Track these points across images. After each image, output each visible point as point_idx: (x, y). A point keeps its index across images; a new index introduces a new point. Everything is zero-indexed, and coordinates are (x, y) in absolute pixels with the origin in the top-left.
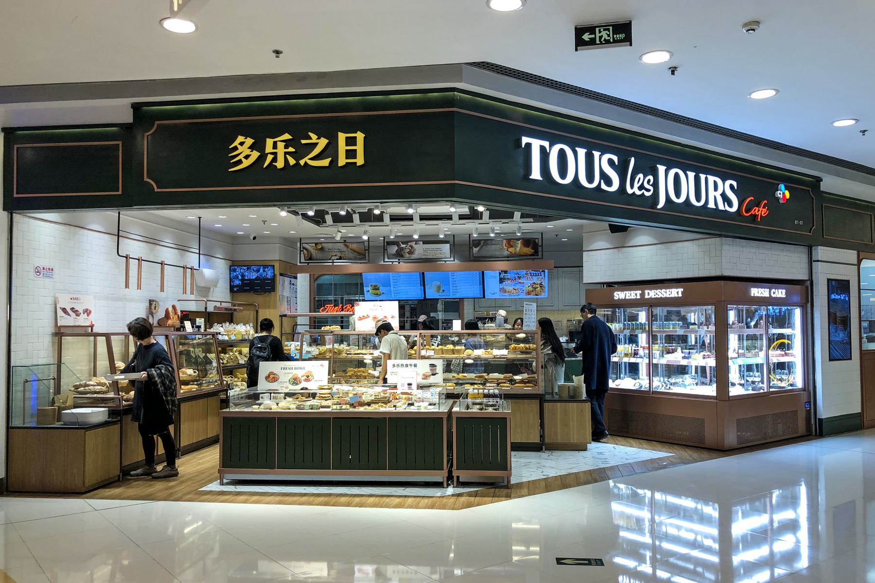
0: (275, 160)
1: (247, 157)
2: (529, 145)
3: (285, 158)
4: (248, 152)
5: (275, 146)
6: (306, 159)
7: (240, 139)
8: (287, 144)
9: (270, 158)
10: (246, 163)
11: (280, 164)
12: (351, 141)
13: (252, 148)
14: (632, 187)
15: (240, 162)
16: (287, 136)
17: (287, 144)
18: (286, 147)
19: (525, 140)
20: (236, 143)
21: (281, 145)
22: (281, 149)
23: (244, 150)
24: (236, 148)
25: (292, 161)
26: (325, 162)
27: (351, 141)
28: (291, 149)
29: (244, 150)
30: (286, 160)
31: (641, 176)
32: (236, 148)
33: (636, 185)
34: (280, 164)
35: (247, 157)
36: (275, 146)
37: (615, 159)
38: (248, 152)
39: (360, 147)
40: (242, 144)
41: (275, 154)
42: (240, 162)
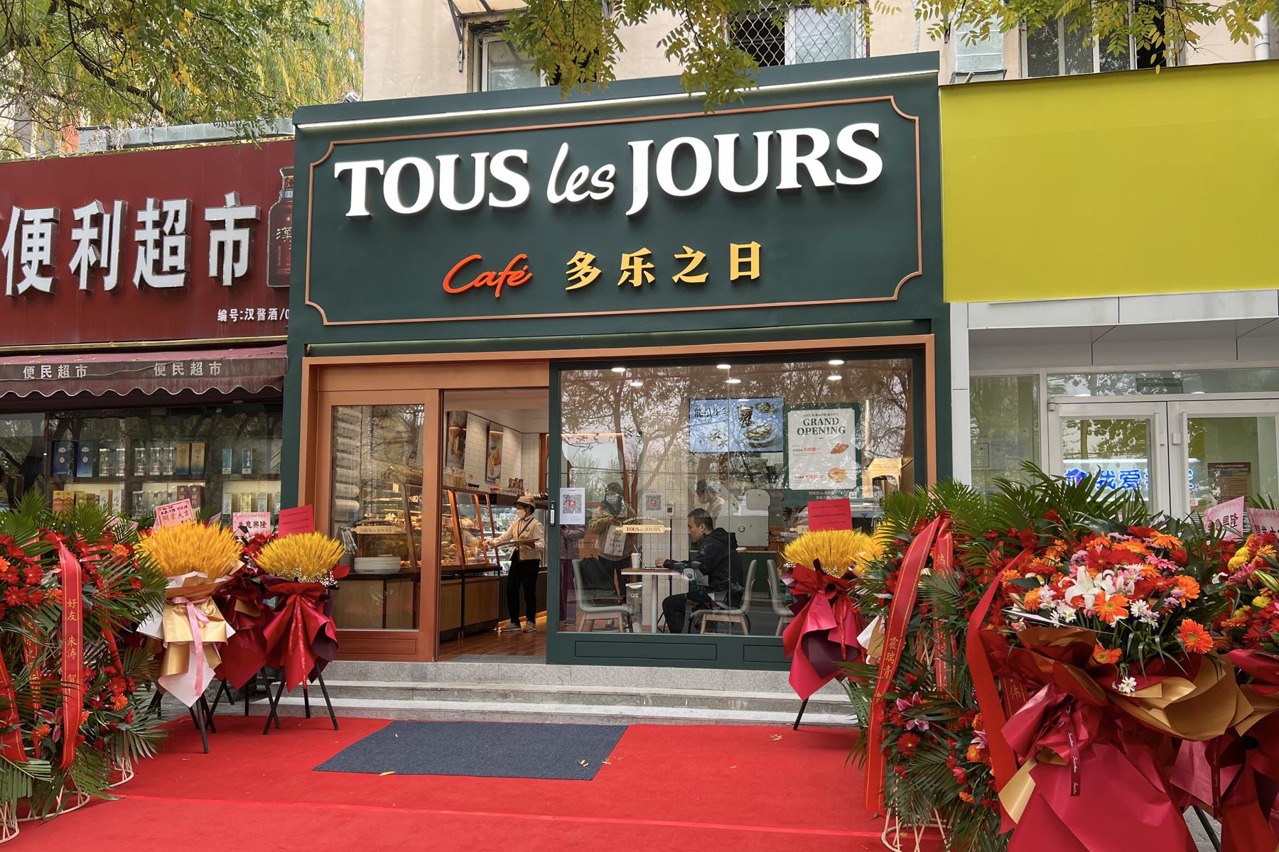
0: (631, 277)
1: (586, 275)
2: (347, 174)
3: (643, 275)
4: (588, 269)
5: (632, 261)
6: (680, 275)
7: (580, 254)
8: (646, 259)
9: (626, 275)
10: (585, 281)
11: (637, 282)
12: (745, 253)
13: (592, 264)
14: (560, 188)
15: (579, 280)
16: (645, 251)
17: (646, 259)
18: (644, 263)
19: (339, 167)
20: (574, 260)
21: (638, 261)
22: (638, 266)
23: (583, 267)
24: (574, 265)
25: (650, 278)
26: (701, 278)
27: (745, 253)
28: (649, 265)
29: (583, 267)
30: (644, 277)
31: (584, 170)
32: (574, 265)
33: (571, 186)
34: (637, 282)
35: (586, 275)
36: (632, 261)
37: (522, 154)
38: (588, 269)
39: (754, 260)
40: (581, 260)
41: (632, 271)
42: (579, 280)
